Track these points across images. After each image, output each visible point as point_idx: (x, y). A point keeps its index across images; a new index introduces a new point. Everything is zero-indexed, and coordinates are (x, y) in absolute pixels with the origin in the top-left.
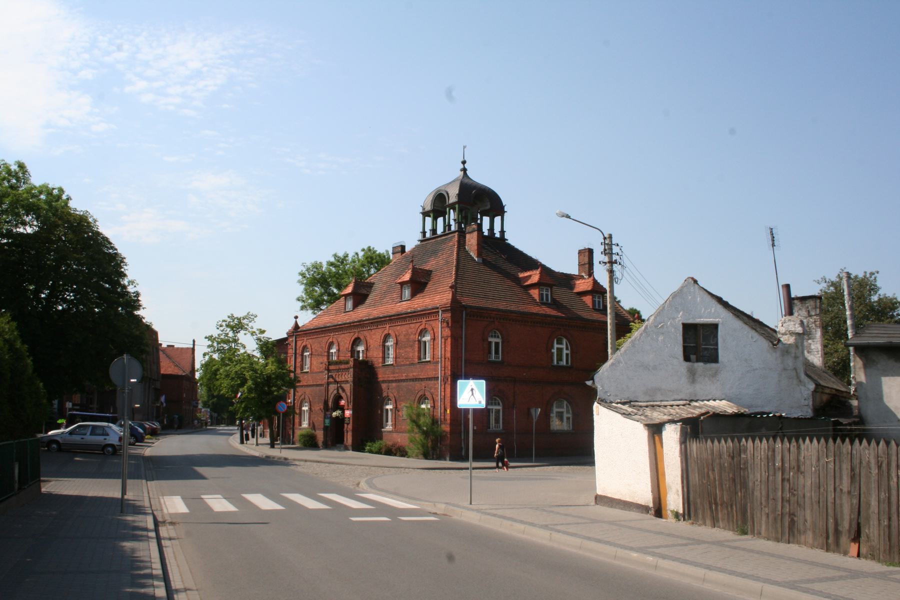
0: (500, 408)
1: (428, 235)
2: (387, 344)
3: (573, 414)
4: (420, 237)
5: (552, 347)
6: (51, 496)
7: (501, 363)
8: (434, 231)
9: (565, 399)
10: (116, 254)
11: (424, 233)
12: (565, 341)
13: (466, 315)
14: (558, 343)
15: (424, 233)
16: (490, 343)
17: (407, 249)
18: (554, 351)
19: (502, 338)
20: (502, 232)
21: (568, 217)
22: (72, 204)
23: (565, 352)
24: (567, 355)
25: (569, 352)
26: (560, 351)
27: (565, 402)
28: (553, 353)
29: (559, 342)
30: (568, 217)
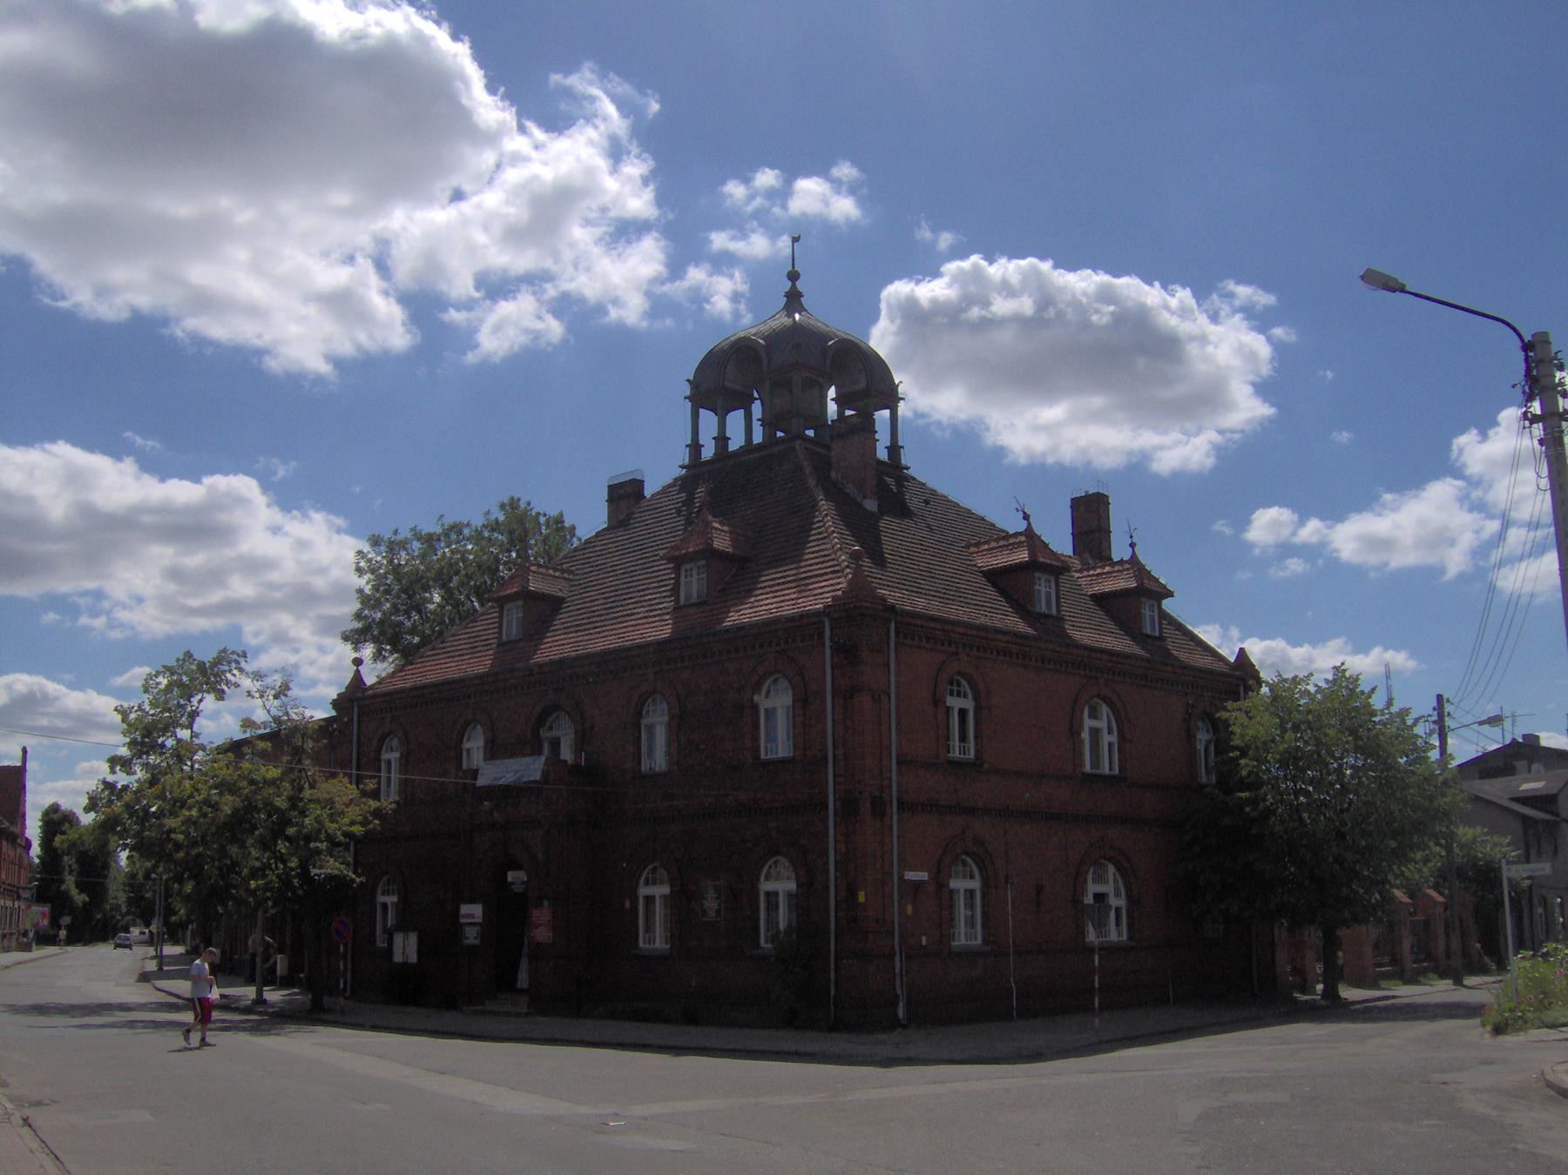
0: (975, 884)
1: (708, 452)
2: (644, 721)
3: (1130, 897)
4: (684, 457)
5: (1084, 891)
6: (1266, 288)
7: (977, 765)
8: (722, 440)
9: (1110, 860)
10: (928, 425)
11: (695, 447)
12: (1105, 709)
13: (897, 633)
14: (1095, 881)
15: (695, 447)
16: (948, 710)
17: (648, 492)
18: (1085, 735)
19: (975, 699)
20: (894, 449)
21: (1393, 286)
22: (688, 393)
23: (1107, 738)
24: (1110, 744)
25: (1114, 739)
26: (1095, 733)
27: (1111, 869)
28: (1082, 741)
29: (1094, 714)
30: (1393, 286)
